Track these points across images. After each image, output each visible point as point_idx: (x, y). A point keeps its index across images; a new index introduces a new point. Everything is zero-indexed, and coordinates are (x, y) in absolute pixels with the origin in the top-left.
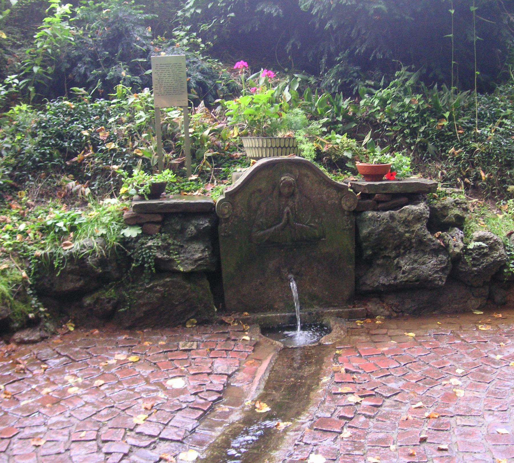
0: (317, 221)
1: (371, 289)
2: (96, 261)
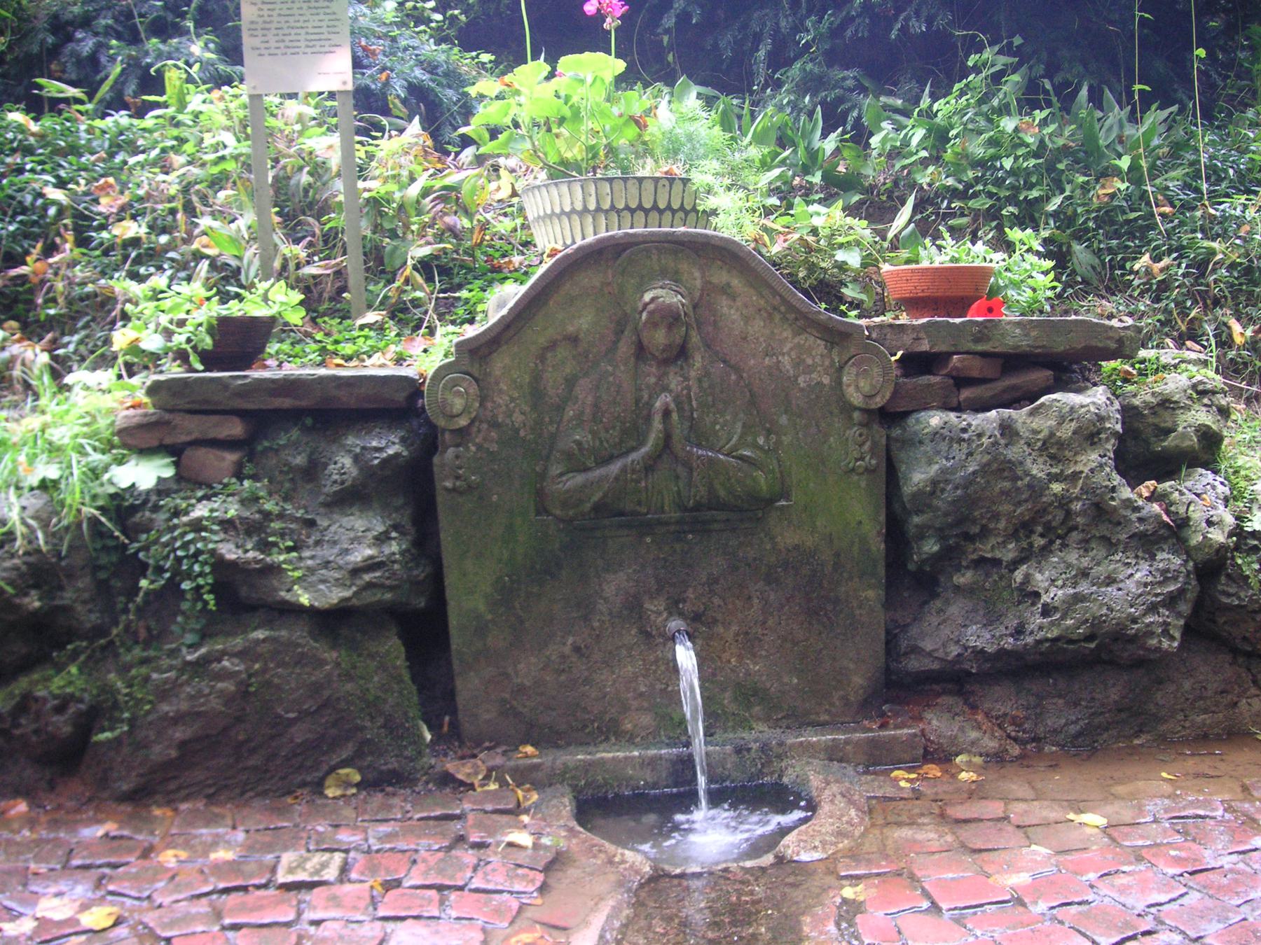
0: (761, 441)
1: (936, 666)
2: (16, 568)
